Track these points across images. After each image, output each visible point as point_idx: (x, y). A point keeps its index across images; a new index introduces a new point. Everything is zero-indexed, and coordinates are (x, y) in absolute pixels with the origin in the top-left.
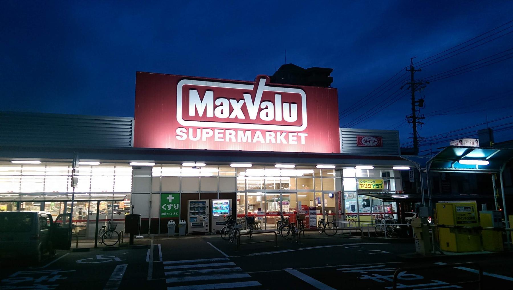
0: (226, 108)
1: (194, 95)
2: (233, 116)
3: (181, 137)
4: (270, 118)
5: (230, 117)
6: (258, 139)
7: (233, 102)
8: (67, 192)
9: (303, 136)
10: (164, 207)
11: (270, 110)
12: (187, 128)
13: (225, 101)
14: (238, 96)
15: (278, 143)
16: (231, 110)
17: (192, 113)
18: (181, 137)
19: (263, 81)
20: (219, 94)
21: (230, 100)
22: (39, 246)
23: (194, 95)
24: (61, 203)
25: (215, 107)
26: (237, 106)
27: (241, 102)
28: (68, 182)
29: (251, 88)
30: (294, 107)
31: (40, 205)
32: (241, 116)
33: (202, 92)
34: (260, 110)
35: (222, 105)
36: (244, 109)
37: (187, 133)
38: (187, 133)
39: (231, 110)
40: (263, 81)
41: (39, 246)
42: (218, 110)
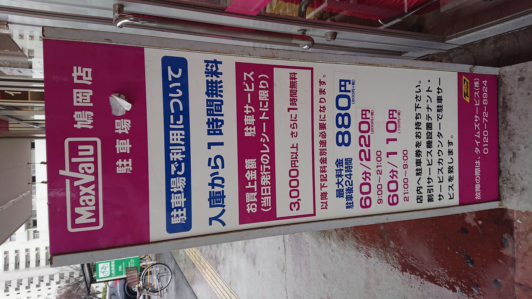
0: (87, 198)
1: (78, 221)
2: (93, 193)
4: (92, 165)
5: (94, 195)
7: (81, 193)
8: (114, 267)
10: (247, 89)
11: (86, 166)
13: (82, 199)
14: (76, 190)
15: (76, 67)
16: (87, 194)
17: (93, 220)
19: (61, 172)
20: (75, 203)
21: (80, 195)
22: (119, 292)
23: (78, 221)
24: (116, 283)
25: (87, 205)
26: (84, 190)
27: (81, 188)
28: (418, 136)
29: (68, 181)
31: (70, 182)
32: (93, 186)
33: (75, 216)
34: (86, 173)
35: (85, 200)
36: (87, 185)
39: (87, 194)
40: (61, 172)
41: (119, 292)
42: (88, 203)
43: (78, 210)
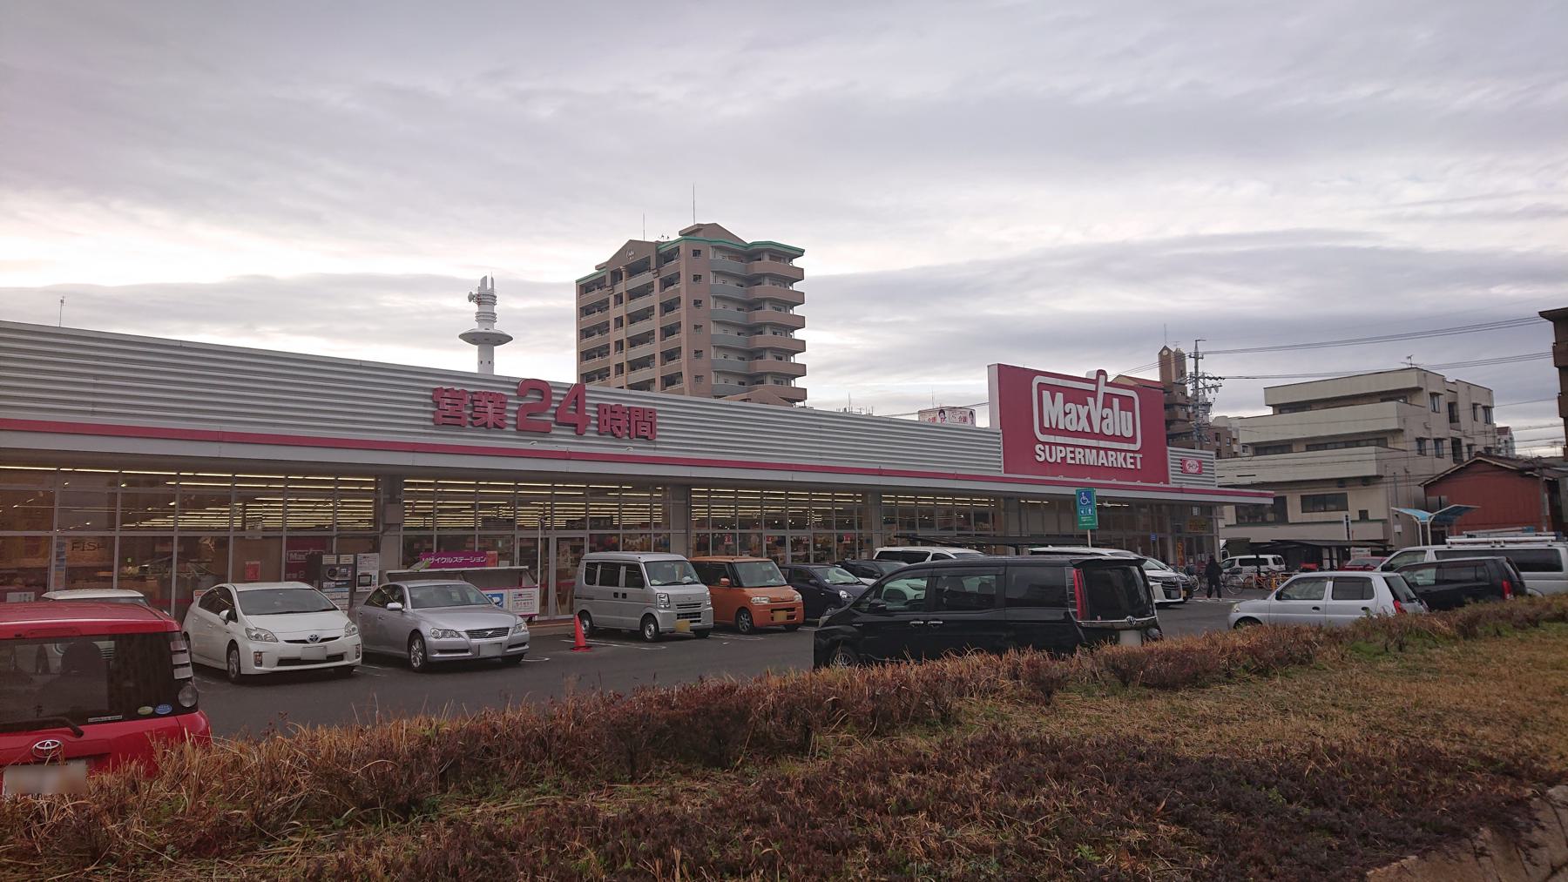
3: (1040, 456)
6: (1103, 462)
9: (1139, 456)
12: (1044, 443)
18: (1040, 456)
30: (1130, 414)
37: (1044, 451)
38: (1044, 451)
43: (1059, 396)
